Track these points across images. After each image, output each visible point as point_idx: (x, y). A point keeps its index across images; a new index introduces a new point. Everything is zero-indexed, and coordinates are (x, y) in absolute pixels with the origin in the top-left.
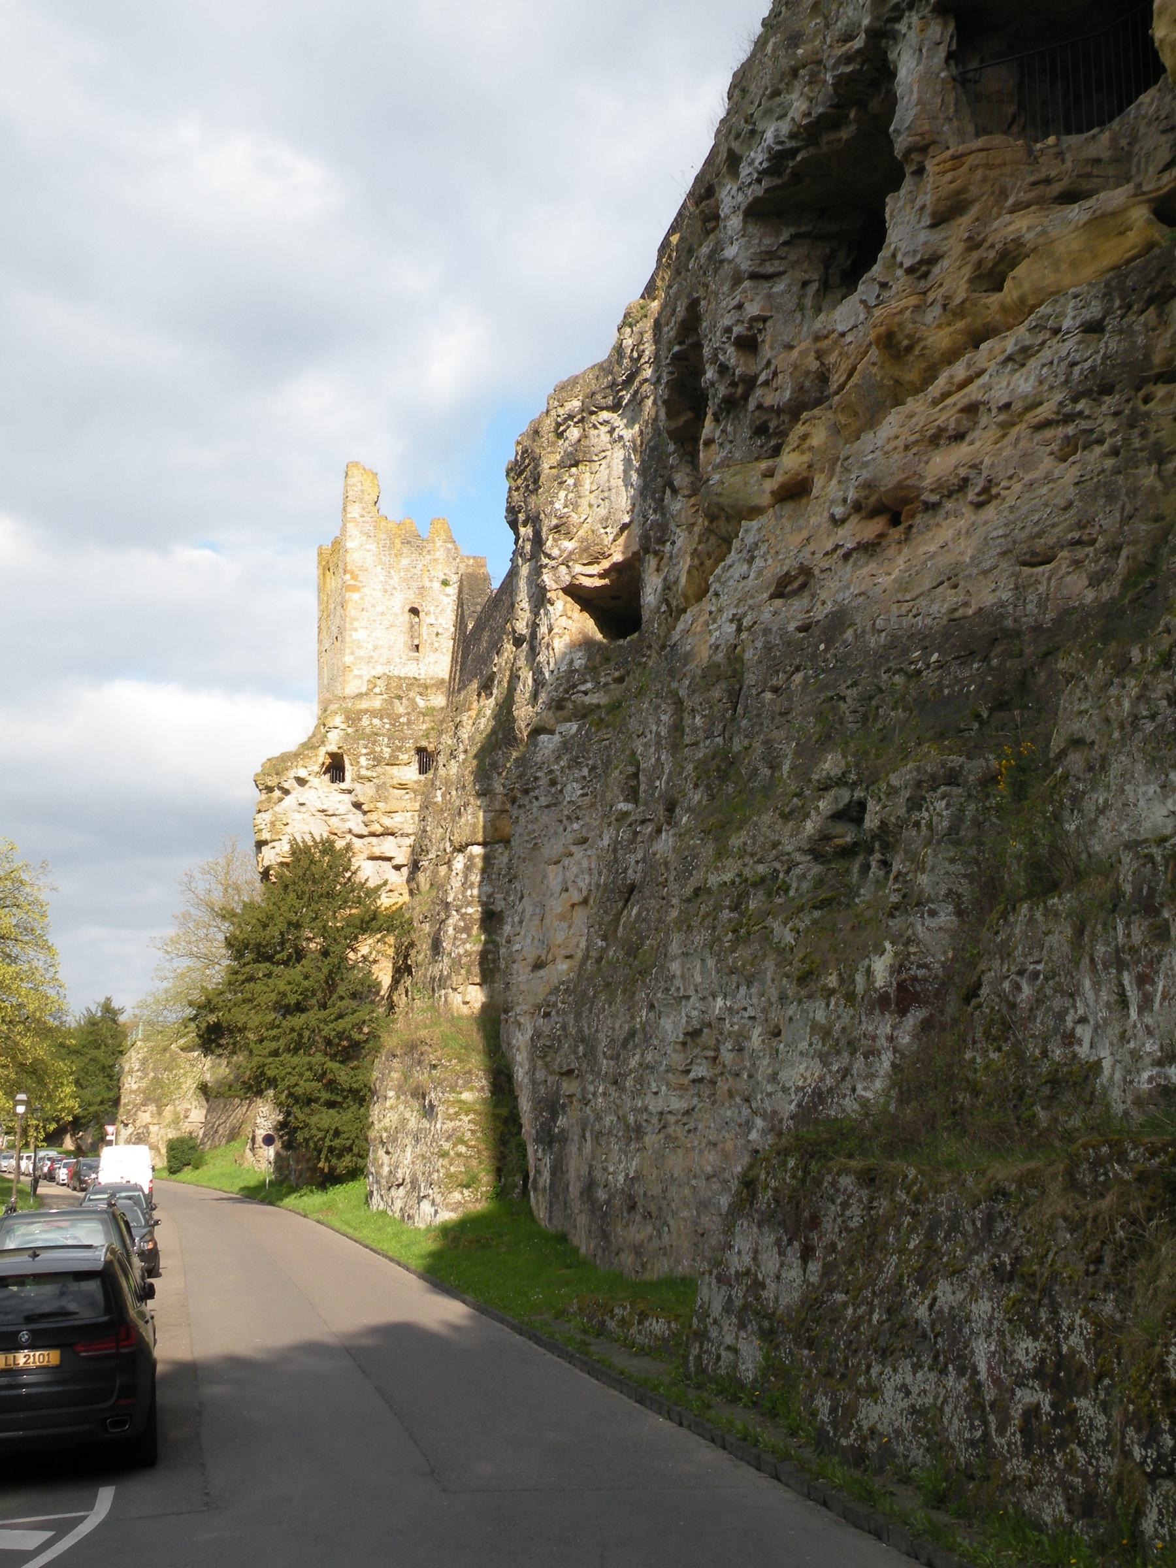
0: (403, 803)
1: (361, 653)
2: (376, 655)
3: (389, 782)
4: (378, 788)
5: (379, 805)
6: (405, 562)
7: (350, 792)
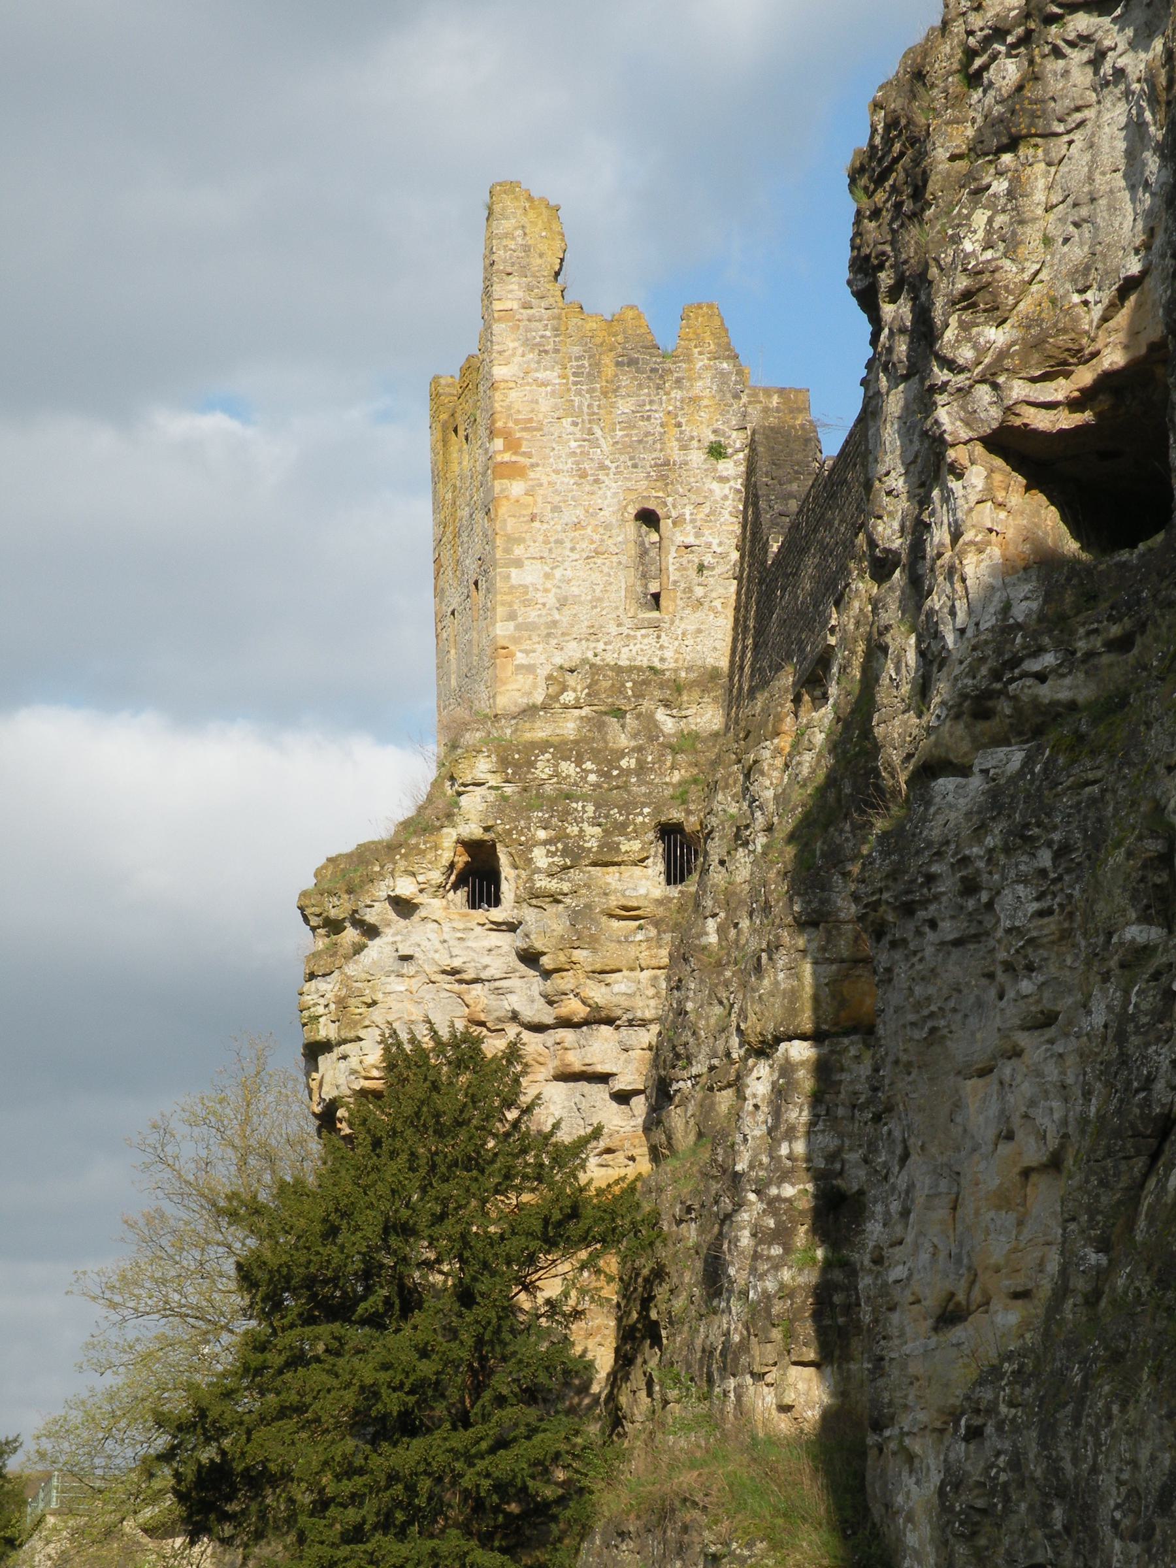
0: (633, 951)
1: (533, 615)
2: (564, 618)
3: (600, 903)
4: (576, 916)
5: (579, 955)
6: (625, 406)
7: (512, 927)
